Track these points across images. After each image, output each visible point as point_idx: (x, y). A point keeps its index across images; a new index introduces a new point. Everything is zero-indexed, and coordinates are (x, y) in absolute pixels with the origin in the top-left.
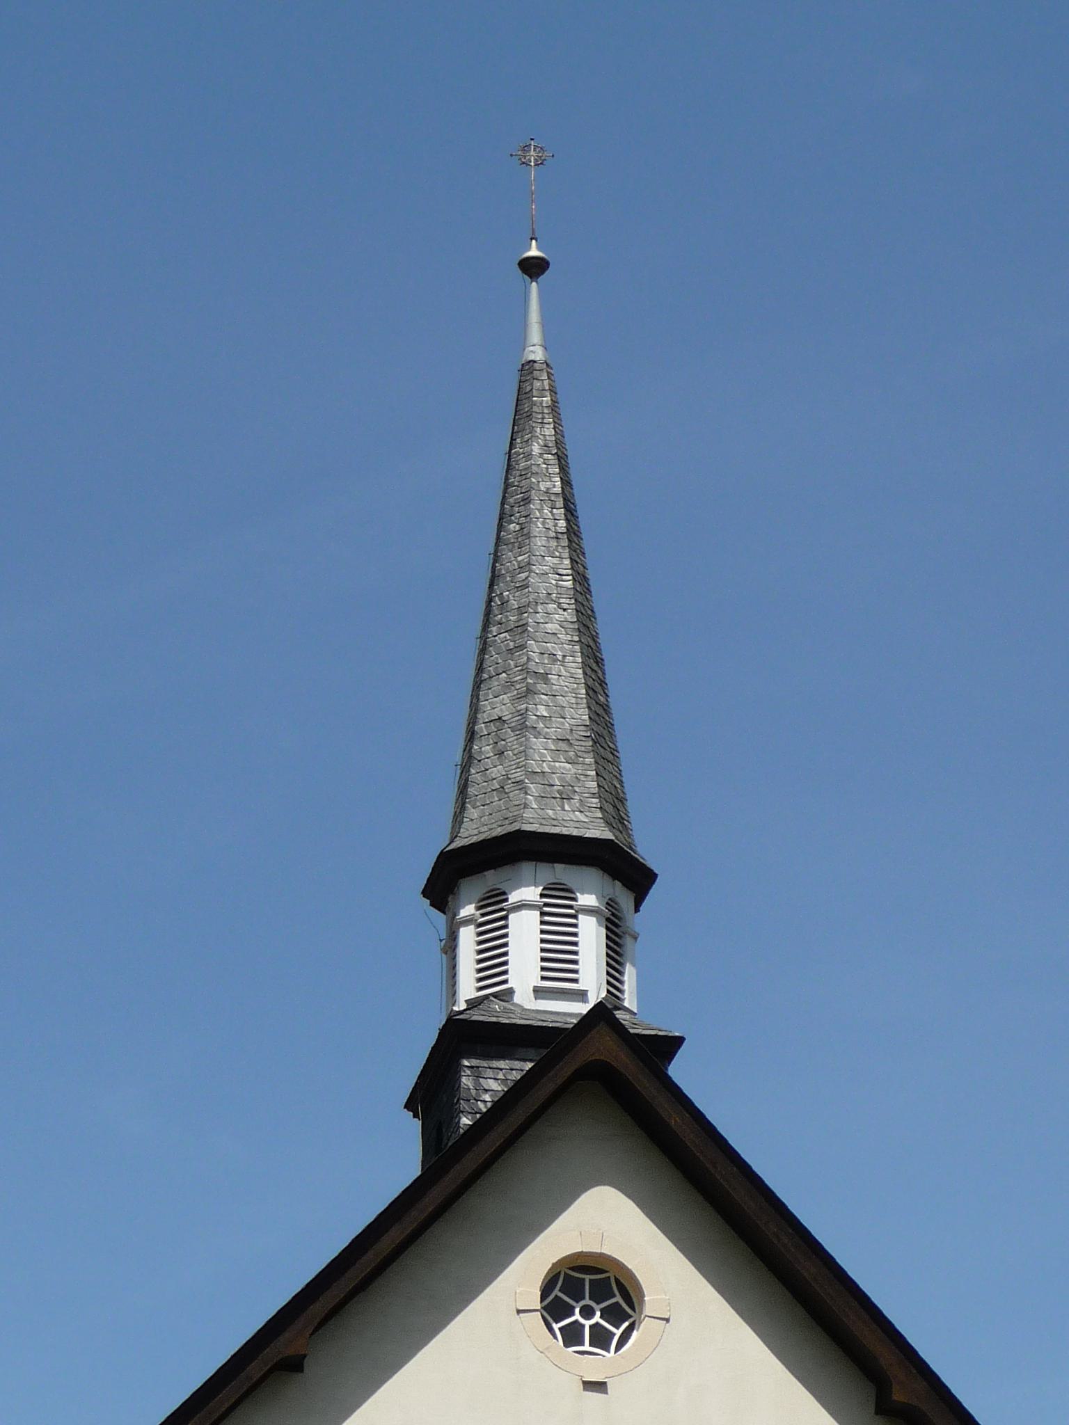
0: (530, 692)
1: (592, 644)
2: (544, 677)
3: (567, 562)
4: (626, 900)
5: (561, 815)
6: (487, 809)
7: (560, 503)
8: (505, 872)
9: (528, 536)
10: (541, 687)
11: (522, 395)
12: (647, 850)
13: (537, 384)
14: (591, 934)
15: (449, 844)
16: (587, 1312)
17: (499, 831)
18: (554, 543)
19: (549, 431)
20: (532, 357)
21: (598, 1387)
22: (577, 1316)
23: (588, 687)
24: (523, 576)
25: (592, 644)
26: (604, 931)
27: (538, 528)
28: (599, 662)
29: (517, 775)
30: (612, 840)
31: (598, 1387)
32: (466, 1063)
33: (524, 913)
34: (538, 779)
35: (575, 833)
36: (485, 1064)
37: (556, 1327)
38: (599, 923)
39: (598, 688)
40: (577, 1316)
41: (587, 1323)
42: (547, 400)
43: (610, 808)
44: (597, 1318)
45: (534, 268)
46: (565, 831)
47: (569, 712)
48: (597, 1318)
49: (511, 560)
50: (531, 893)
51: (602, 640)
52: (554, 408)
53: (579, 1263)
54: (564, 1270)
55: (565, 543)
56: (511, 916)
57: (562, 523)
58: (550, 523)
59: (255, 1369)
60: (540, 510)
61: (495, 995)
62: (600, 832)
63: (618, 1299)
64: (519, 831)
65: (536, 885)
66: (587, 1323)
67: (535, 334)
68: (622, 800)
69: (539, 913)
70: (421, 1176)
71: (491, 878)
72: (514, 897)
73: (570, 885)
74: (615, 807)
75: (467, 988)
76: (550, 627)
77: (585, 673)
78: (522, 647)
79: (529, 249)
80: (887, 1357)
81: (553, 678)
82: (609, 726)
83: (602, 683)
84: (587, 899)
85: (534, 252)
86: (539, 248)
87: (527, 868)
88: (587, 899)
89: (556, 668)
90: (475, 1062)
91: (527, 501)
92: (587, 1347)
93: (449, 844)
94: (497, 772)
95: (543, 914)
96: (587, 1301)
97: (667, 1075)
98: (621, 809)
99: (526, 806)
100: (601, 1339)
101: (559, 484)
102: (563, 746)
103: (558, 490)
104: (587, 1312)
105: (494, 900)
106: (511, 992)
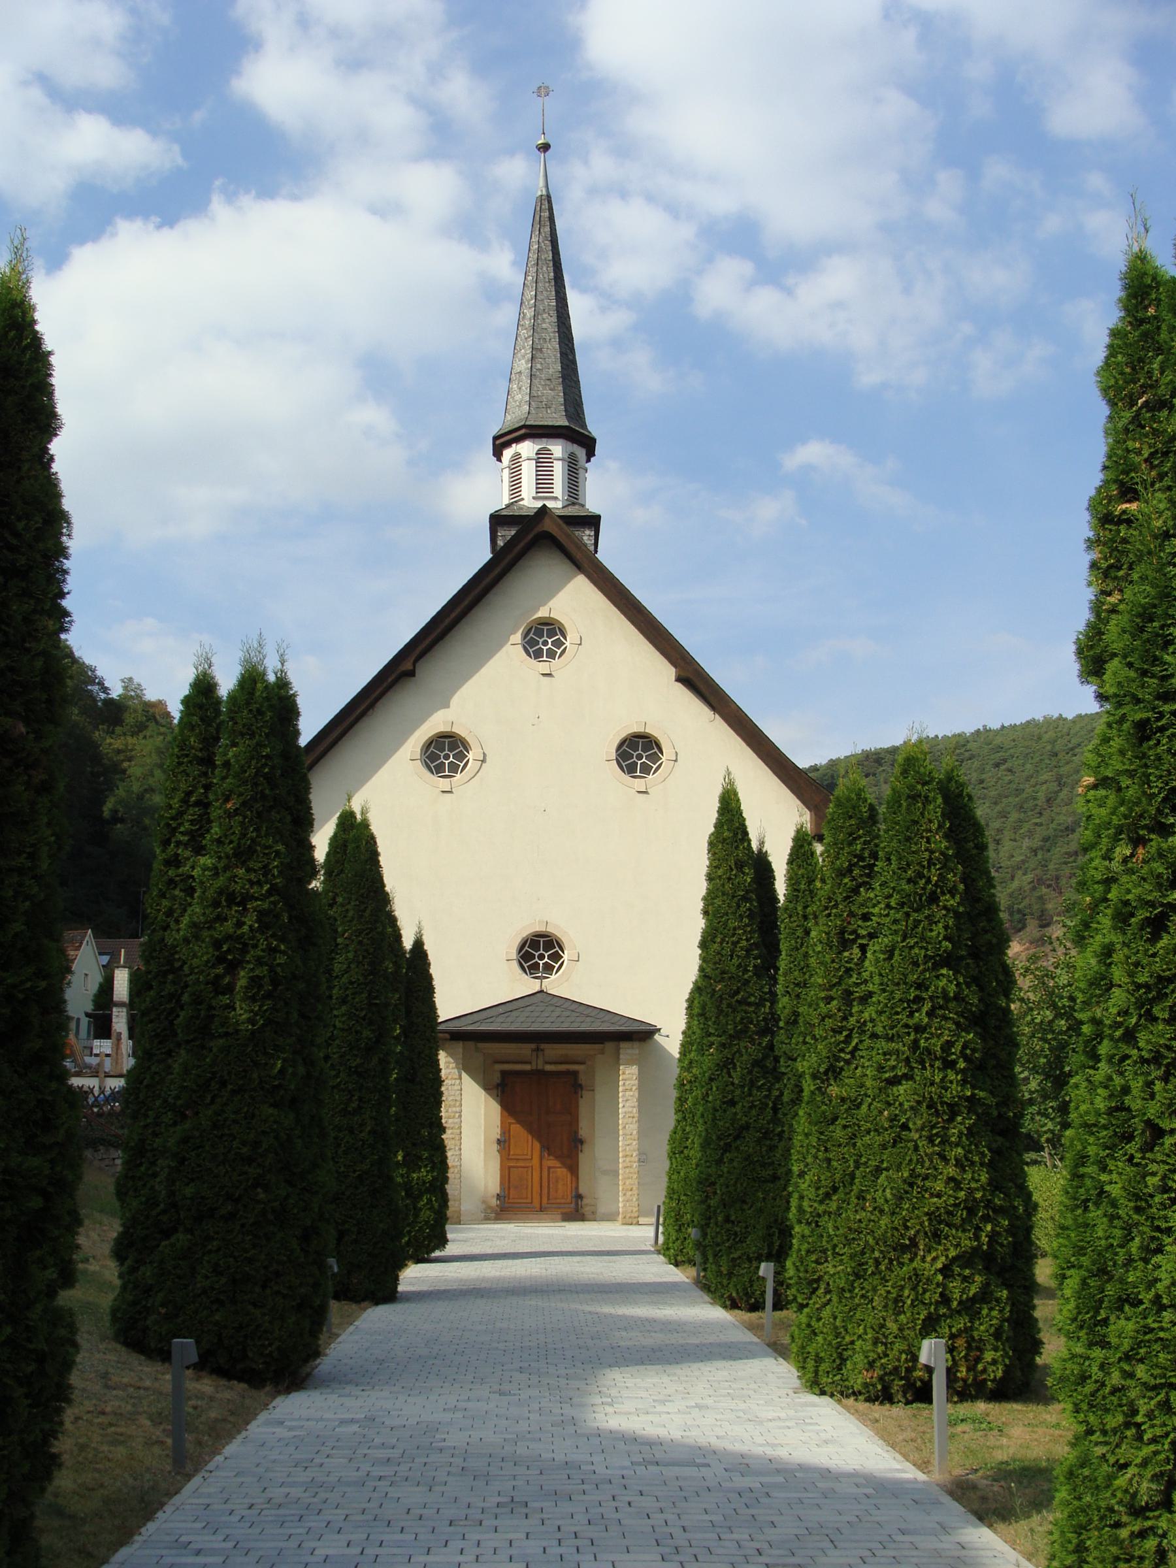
4: (581, 453)
7: (551, 264)
18: (547, 285)
22: (545, 648)
40: (545, 648)
41: (550, 646)
44: (550, 641)
54: (553, 938)
55: (553, 283)
57: (552, 274)
58: (546, 276)
62: (564, 422)
66: (550, 646)
69: (600, 1056)
70: (491, 560)
76: (544, 326)
81: (544, 350)
87: (561, 441)
96: (541, 641)
97: (675, 667)
101: (551, 255)
102: (548, 382)
103: (551, 258)
104: (546, 643)
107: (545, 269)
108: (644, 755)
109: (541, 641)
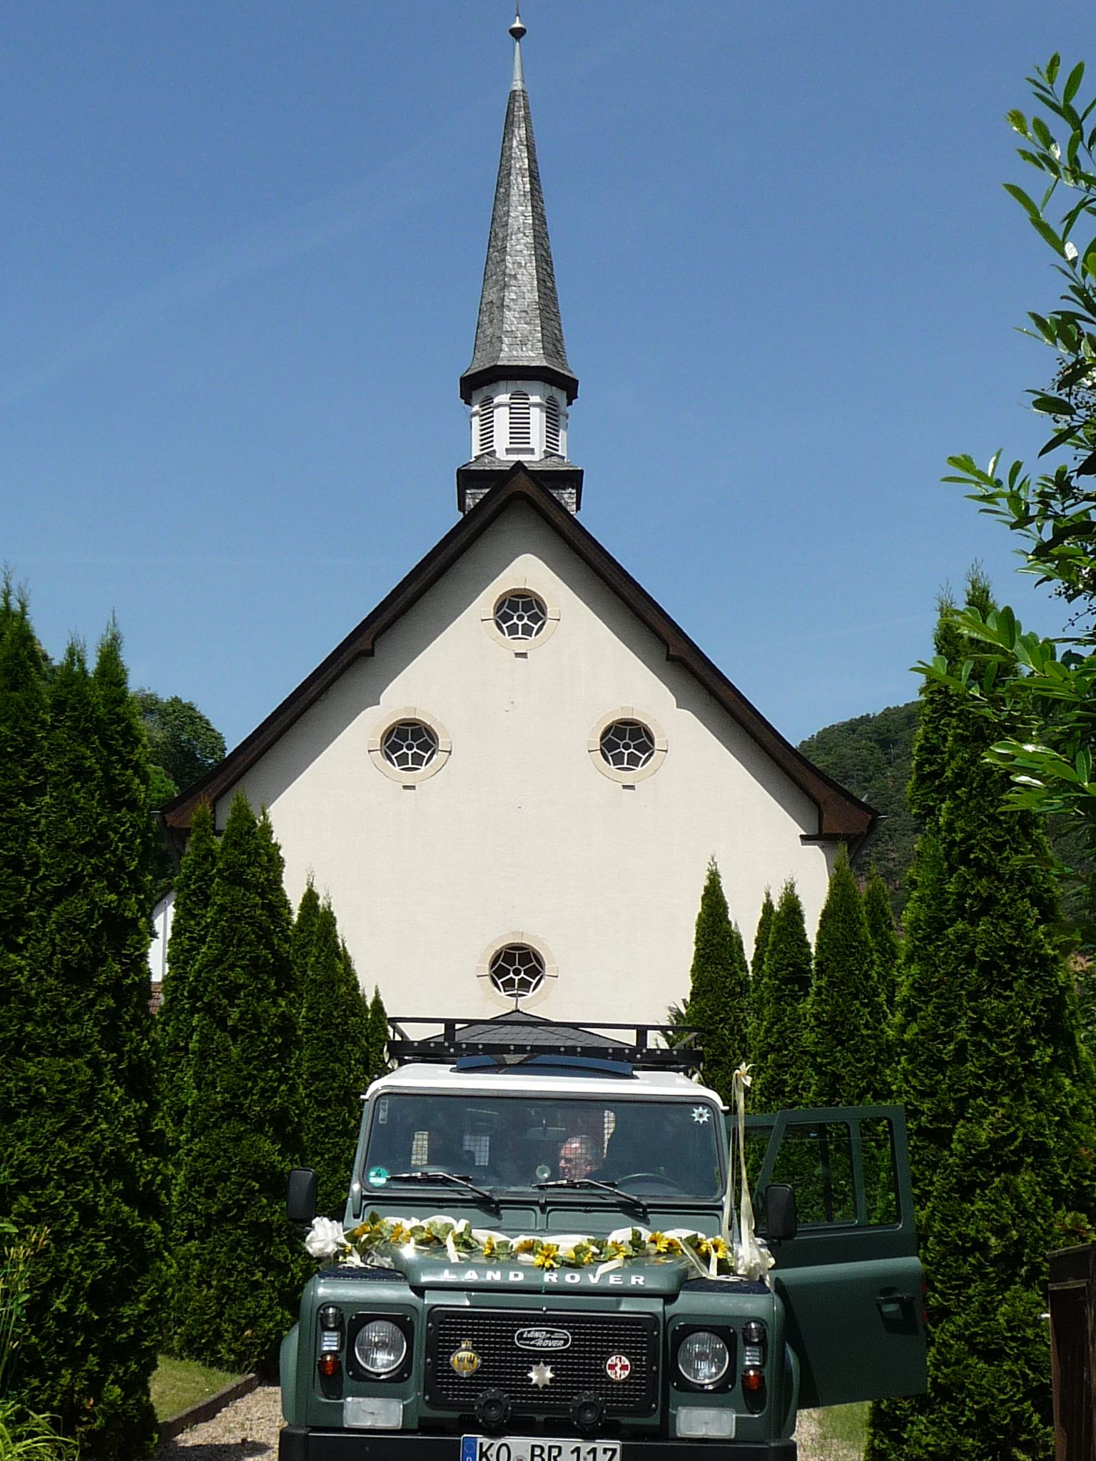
0: (505, 286)
1: (544, 253)
2: (515, 277)
3: (530, 208)
4: (561, 397)
5: (521, 353)
6: (484, 353)
8: (493, 386)
9: (509, 196)
10: (513, 282)
11: (510, 112)
12: (574, 367)
13: (517, 104)
14: (537, 418)
15: (1072, 300)
16: (520, 618)
17: (487, 366)
18: (522, 198)
19: (523, 132)
20: (516, 88)
21: (524, 655)
22: (515, 620)
23: (538, 280)
24: (505, 219)
25: (544, 253)
26: (544, 415)
27: (514, 191)
28: (549, 264)
29: (498, 333)
30: (546, 367)
31: (524, 655)
32: (468, 491)
33: (501, 409)
34: (508, 334)
35: (526, 364)
36: (479, 491)
37: (504, 626)
38: (542, 411)
39: (547, 279)
40: (515, 620)
41: (520, 623)
42: (522, 113)
43: (550, 347)
44: (525, 621)
45: (518, 34)
46: (521, 364)
47: (527, 295)
48: (525, 621)
49: (502, 209)
50: (503, 398)
51: (552, 250)
52: (527, 118)
53: (517, 593)
55: (529, 197)
56: (495, 411)
57: (528, 186)
58: (521, 186)
59: (345, 658)
60: (516, 180)
61: (487, 454)
63: (537, 610)
64: (495, 366)
65: (507, 393)
67: (518, 75)
68: (560, 341)
71: (486, 390)
72: (496, 400)
73: (526, 392)
74: (554, 345)
75: (476, 451)
76: (518, 248)
77: (537, 272)
78: (504, 260)
79: (515, 22)
80: (666, 632)
82: (555, 301)
83: (551, 275)
84: (535, 399)
85: (517, 25)
86: (521, 22)
87: (502, 384)
88: (535, 399)
89: (520, 271)
90: (473, 491)
91: (509, 174)
92: (520, 635)
93: (1072, 300)
94: (488, 332)
95: (511, 408)
96: (521, 613)
98: (559, 345)
99: (501, 350)
100: (527, 631)
102: (524, 314)
103: (527, 166)
105: (487, 401)
106: (494, 451)
107: (519, 179)
108: (522, 975)
109: (521, 613)
